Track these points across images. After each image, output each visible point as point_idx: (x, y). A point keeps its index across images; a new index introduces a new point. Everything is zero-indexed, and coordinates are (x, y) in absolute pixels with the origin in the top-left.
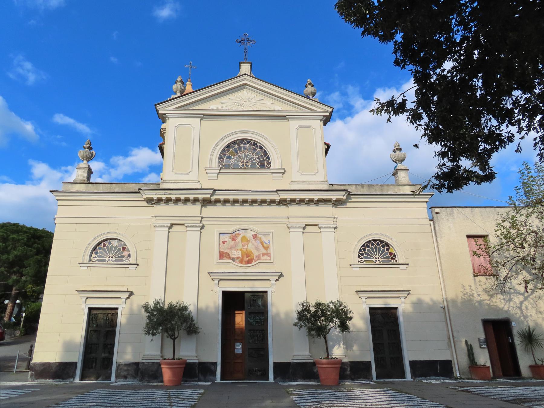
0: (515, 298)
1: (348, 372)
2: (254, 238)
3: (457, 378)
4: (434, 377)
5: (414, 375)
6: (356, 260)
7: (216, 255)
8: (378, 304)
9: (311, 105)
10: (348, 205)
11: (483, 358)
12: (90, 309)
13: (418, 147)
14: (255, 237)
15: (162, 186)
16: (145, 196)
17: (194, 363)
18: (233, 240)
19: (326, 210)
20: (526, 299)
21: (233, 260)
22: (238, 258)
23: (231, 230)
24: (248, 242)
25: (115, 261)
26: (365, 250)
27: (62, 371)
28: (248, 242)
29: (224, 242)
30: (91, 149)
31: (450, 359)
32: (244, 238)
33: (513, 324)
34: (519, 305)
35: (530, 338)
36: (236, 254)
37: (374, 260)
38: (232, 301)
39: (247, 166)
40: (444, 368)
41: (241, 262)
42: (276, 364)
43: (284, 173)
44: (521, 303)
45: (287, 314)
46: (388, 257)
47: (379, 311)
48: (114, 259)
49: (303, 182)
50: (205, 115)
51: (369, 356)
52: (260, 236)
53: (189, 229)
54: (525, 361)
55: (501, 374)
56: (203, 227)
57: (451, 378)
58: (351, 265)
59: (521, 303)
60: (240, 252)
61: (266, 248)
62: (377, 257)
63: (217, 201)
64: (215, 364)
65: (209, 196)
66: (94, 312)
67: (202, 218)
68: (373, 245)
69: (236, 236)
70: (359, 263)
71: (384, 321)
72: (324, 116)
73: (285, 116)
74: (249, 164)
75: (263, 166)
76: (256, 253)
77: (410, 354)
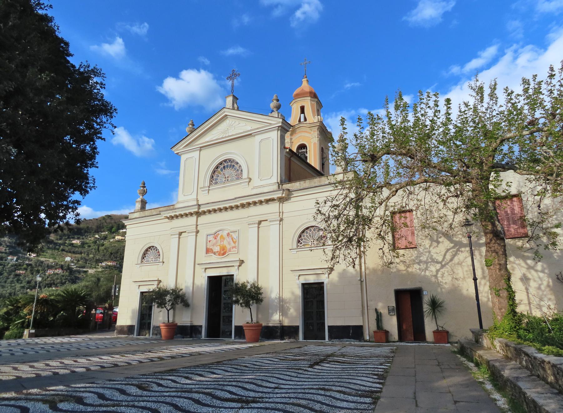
0: (432, 267)
1: (279, 334)
2: (228, 235)
3: (366, 341)
4: (346, 339)
5: (331, 337)
8: (312, 279)
9: (268, 119)
10: (292, 199)
11: (391, 324)
12: (142, 293)
13: (536, 75)
14: (228, 234)
15: (177, 206)
17: (188, 326)
19: (274, 207)
20: (443, 267)
21: (215, 254)
22: (217, 252)
23: (213, 231)
24: (224, 239)
27: (130, 329)
28: (224, 239)
30: (144, 187)
31: (361, 324)
32: (222, 236)
33: (425, 293)
34: (435, 274)
35: (435, 305)
36: (217, 249)
38: (216, 284)
40: (355, 333)
42: (235, 326)
44: (438, 271)
45: (202, 285)
46: (157, 258)
47: (316, 286)
50: (201, 147)
51: (299, 322)
52: (231, 234)
54: (430, 327)
55: (413, 338)
56: (197, 232)
57: (360, 341)
59: (438, 271)
61: (235, 242)
64: (201, 326)
65: (196, 210)
66: (144, 294)
69: (217, 236)
71: (313, 294)
72: (279, 127)
73: (251, 134)
74: (229, 179)
76: (228, 247)
77: (330, 321)
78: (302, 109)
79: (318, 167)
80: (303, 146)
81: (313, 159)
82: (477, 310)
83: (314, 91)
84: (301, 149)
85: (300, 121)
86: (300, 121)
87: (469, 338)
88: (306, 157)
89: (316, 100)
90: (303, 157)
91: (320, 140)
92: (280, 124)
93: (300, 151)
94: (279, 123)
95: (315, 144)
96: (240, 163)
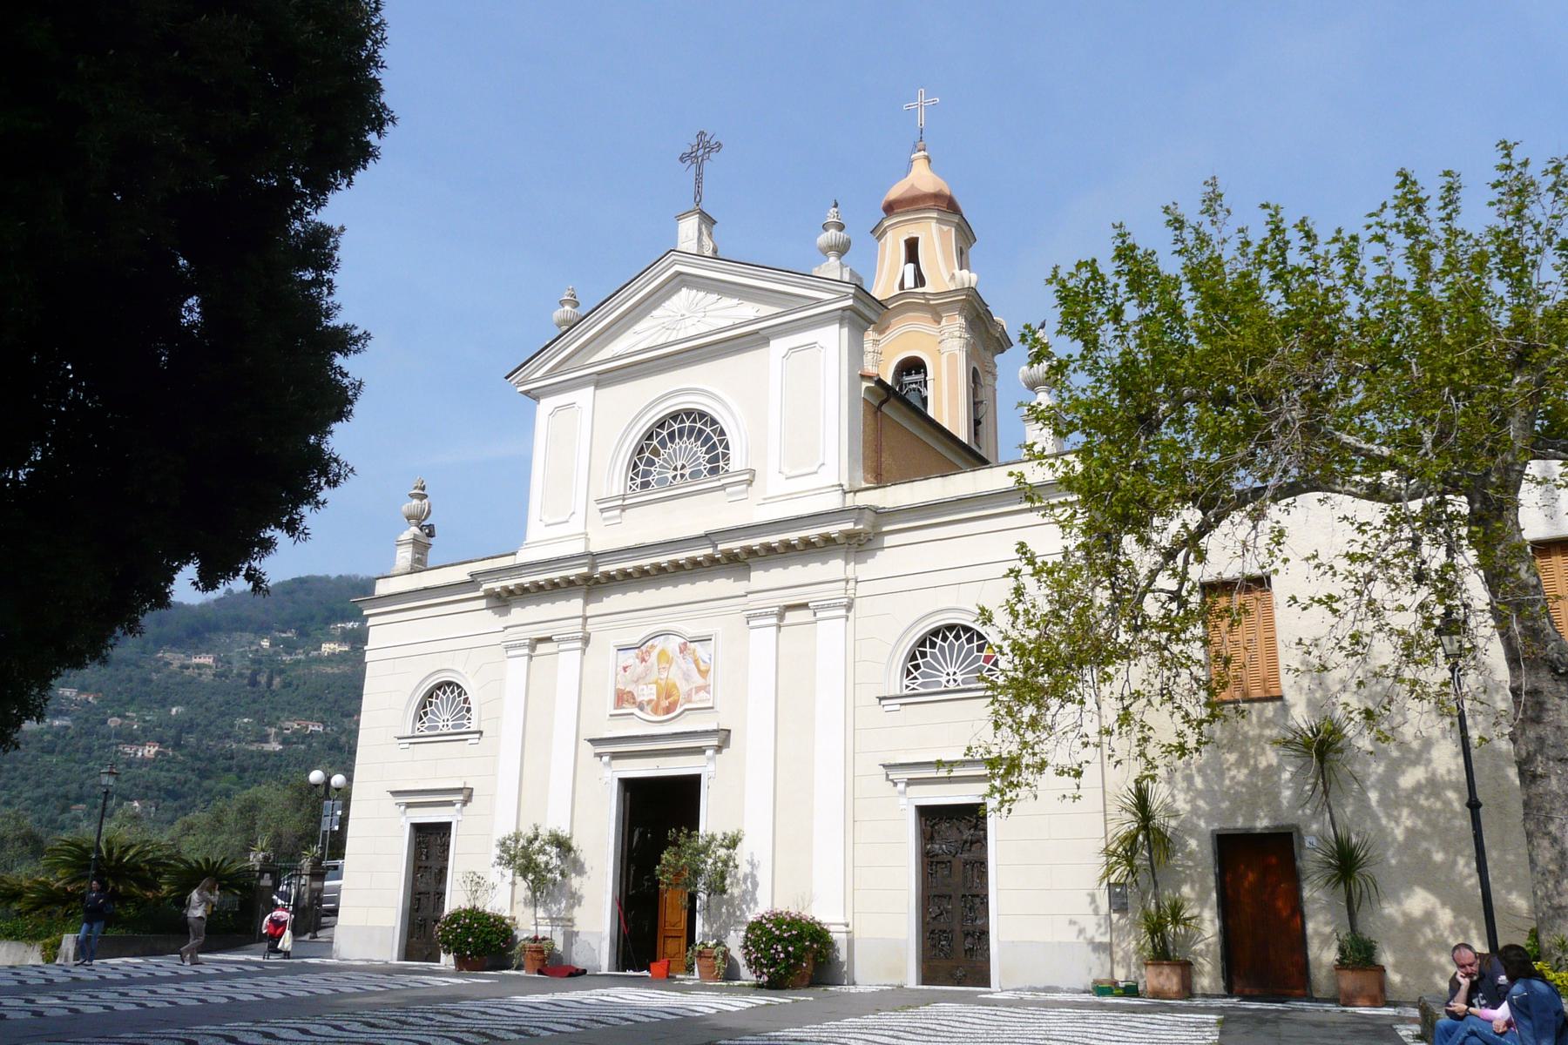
6: (895, 683)
7: (610, 698)
14: (683, 649)
16: (485, 586)
18: (643, 660)
22: (649, 702)
24: (670, 661)
25: (964, 682)
26: (923, 655)
28: (670, 661)
29: (625, 669)
32: (662, 653)
36: (647, 693)
37: (944, 679)
39: (682, 476)
41: (655, 711)
43: (750, 483)
48: (959, 678)
49: (790, 496)
53: (563, 647)
58: (881, 699)
60: (654, 687)
61: (704, 674)
62: (951, 671)
63: (609, 578)
65: (585, 570)
67: (586, 618)
68: (933, 645)
70: (906, 692)
72: (844, 309)
75: (714, 471)
76: (683, 687)
78: (912, 247)
79: (963, 434)
80: (913, 366)
81: (947, 404)
83: (947, 191)
84: (909, 374)
88: (924, 400)
89: (956, 219)
91: (967, 345)
92: (850, 302)
93: (907, 379)
94: (845, 297)
95: (952, 357)
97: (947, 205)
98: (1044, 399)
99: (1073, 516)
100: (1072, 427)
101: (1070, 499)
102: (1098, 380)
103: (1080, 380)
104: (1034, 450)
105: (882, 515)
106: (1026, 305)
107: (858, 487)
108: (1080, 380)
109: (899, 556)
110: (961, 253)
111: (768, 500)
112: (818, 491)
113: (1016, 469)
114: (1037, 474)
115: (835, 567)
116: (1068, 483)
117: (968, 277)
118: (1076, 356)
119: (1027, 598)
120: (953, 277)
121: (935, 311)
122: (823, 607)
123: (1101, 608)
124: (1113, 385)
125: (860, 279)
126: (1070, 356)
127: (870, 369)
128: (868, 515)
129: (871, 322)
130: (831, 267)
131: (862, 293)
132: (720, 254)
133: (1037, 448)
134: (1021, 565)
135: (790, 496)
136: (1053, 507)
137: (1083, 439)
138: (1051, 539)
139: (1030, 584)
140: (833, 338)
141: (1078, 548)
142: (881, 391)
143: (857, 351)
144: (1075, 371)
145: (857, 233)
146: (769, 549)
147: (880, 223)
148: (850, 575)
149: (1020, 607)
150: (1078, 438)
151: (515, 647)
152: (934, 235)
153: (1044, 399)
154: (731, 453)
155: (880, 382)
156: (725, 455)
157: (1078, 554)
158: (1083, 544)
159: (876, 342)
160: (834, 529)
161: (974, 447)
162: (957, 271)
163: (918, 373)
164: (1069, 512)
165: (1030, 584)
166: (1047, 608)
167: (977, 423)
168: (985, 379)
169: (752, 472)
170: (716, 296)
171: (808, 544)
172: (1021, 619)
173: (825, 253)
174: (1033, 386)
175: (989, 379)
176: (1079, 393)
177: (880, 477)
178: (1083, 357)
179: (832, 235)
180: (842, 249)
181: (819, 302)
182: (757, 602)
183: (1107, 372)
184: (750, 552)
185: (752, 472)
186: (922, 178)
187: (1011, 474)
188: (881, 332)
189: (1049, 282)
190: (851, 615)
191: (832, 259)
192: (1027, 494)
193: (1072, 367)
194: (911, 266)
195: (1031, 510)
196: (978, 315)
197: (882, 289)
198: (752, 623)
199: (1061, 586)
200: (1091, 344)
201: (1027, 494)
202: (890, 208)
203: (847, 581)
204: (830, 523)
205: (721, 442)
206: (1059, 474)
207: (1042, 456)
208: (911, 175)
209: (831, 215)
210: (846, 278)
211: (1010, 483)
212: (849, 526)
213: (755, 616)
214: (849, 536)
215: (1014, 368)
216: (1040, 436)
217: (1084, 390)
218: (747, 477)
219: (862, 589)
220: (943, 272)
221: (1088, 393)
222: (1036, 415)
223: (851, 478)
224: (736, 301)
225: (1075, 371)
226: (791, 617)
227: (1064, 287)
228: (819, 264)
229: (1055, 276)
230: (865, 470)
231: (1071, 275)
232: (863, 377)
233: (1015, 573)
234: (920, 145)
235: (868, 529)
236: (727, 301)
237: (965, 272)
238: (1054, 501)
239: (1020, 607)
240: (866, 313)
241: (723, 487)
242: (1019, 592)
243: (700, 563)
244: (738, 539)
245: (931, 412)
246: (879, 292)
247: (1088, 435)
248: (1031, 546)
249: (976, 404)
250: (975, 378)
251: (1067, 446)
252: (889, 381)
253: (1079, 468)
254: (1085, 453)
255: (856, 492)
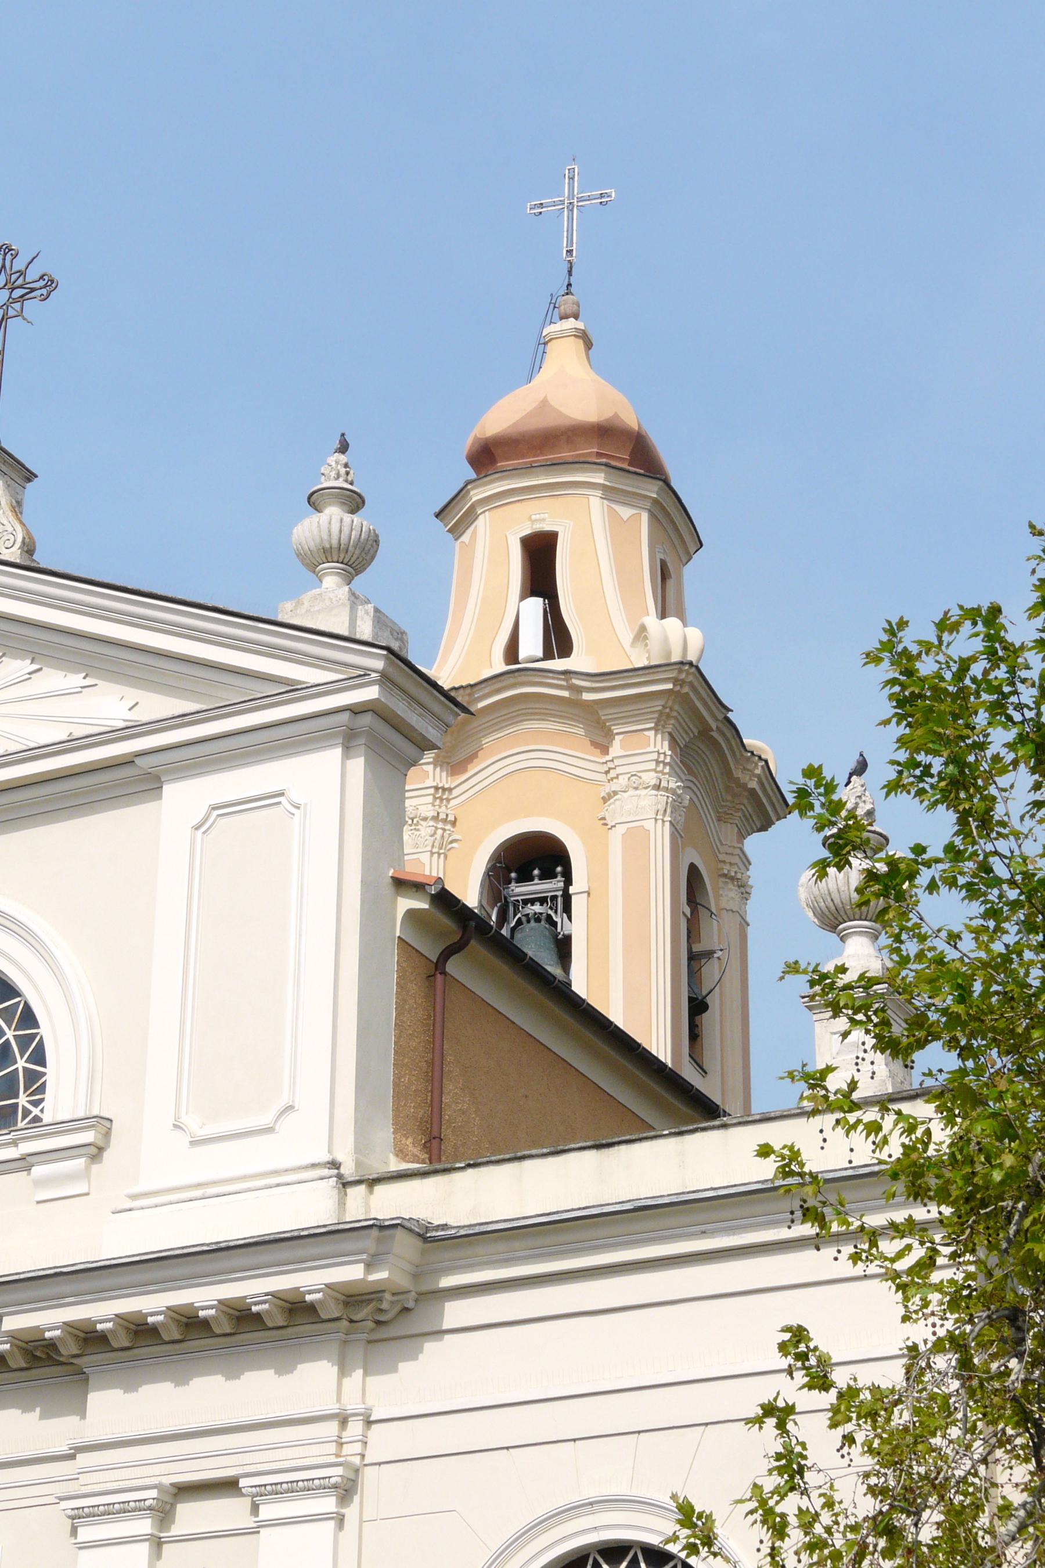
43: (96, 1152)
49: (204, 1191)
72: (355, 710)
78: (540, 558)
79: (659, 1040)
80: (536, 857)
81: (620, 960)
82: (231, 609)
83: (630, 419)
84: (525, 877)
85: (512, 652)
86: (512, 652)
87: (661, 807)
88: (563, 947)
89: (652, 489)
90: (535, 947)
91: (676, 806)
92: (371, 693)
93: (519, 890)
94: (359, 678)
95: (636, 839)
96: (45, 1030)
97: (630, 456)
98: (861, 955)
99: (929, 1263)
100: (921, 1031)
101: (920, 1213)
102: (992, 913)
103: (945, 911)
104: (830, 1089)
105: (435, 1242)
106: (820, 718)
107: (379, 1168)
108: (945, 911)
109: (479, 1356)
110: (664, 574)
111: (141, 1200)
112: (275, 1179)
113: (778, 1134)
114: (830, 1149)
115: (313, 1382)
116: (913, 1176)
117: (677, 637)
118: (935, 850)
119: (811, 1478)
120: (641, 634)
121: (594, 716)
122: (277, 1492)
123: (1005, 1510)
124: (1029, 927)
125: (400, 635)
126: (919, 849)
127: (422, 860)
128: (404, 1245)
129: (424, 745)
130: (328, 603)
131: (402, 668)
132: (41, 559)
133: (835, 1083)
134: (791, 1390)
135: (204, 1191)
136: (873, 1236)
137: (951, 1061)
138: (872, 1325)
139: (816, 1434)
140: (326, 783)
141: (938, 1347)
142: (446, 922)
143: (386, 817)
144: (932, 887)
145: (401, 520)
146: (141, 1331)
147: (460, 494)
148: (352, 1403)
149: (790, 1505)
150: (937, 1059)
151: (109, 1513)
152: (597, 532)
153: (861, 955)
154: (52, 1073)
155: (445, 900)
156: (32, 1077)
157: (941, 1362)
158: (951, 1337)
159: (441, 793)
160: (311, 1280)
161: (689, 1074)
162: (651, 620)
163: (548, 874)
164: (918, 1253)
165: (816, 1434)
166: (869, 1506)
167: (697, 1007)
168: (719, 896)
169: (104, 1124)
170: (25, 666)
171: (243, 1317)
172: (796, 1536)
173: (313, 567)
174: (833, 919)
175: (730, 895)
176: (941, 944)
177: (437, 1149)
178: (953, 853)
179: (332, 521)
180: (354, 558)
181: (293, 690)
182: (100, 1474)
183: (1013, 894)
184: (90, 1338)
185: (104, 1124)
186: (570, 386)
187: (765, 1151)
188: (456, 766)
189: (872, 658)
190: (351, 1512)
191: (331, 582)
192: (808, 1202)
193: (925, 876)
194: (536, 605)
195: (816, 1243)
196: (705, 732)
197: (458, 660)
198: (86, 1534)
199: (894, 1452)
200: (979, 822)
201: (808, 1202)
202: (486, 457)
203: (343, 1420)
204: (300, 1264)
205: (24, 1042)
206: (895, 1149)
207: (849, 1101)
208: (539, 379)
209: (331, 471)
210: (365, 630)
211: (767, 1170)
212: (352, 1273)
213: (94, 1515)
214: (352, 1298)
215: (784, 869)
216: (847, 1054)
217: (954, 938)
218: (88, 1137)
219: (383, 1442)
220: (615, 623)
221: (967, 943)
222: (829, 993)
223: (361, 1146)
224: (76, 680)
225: (932, 887)
226: (192, 1516)
227: (909, 673)
228: (295, 594)
229: (888, 646)
230: (399, 1127)
231: (927, 647)
232: (401, 884)
233: (778, 1414)
234: (566, 304)
235: (404, 1282)
236: (55, 679)
237: (672, 623)
238: (876, 1220)
239: (790, 1505)
240: (412, 719)
241: (24, 1163)
242: (791, 1466)
243: (204, 1325)
244: (56, 1301)
245: (579, 986)
246: (447, 673)
247: (965, 1052)
248: (821, 1339)
249: (694, 959)
250: (693, 889)
251: (916, 1079)
252: (471, 896)
253: (942, 1136)
254: (956, 1097)
255: (373, 1183)
